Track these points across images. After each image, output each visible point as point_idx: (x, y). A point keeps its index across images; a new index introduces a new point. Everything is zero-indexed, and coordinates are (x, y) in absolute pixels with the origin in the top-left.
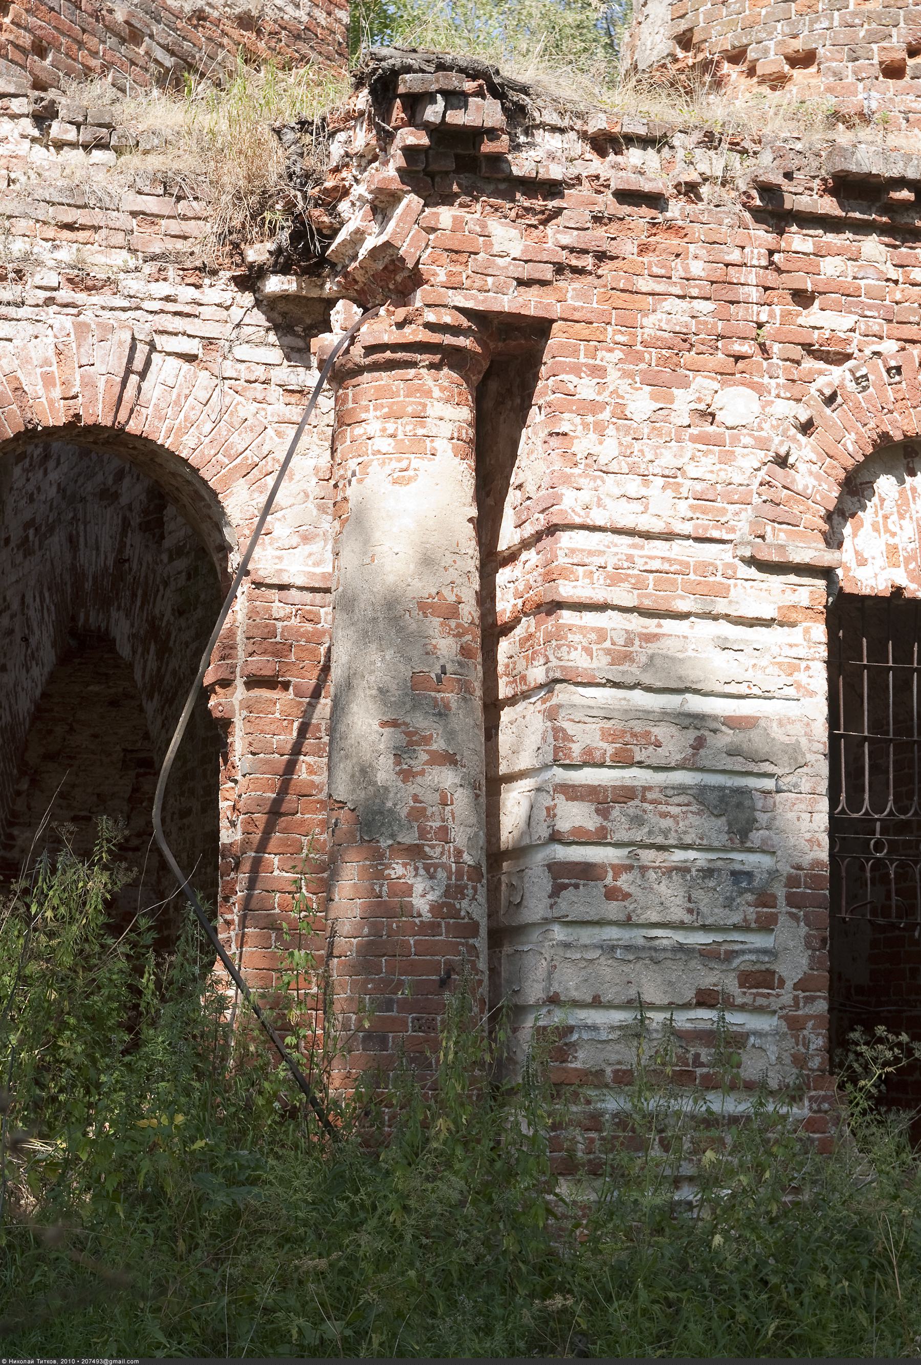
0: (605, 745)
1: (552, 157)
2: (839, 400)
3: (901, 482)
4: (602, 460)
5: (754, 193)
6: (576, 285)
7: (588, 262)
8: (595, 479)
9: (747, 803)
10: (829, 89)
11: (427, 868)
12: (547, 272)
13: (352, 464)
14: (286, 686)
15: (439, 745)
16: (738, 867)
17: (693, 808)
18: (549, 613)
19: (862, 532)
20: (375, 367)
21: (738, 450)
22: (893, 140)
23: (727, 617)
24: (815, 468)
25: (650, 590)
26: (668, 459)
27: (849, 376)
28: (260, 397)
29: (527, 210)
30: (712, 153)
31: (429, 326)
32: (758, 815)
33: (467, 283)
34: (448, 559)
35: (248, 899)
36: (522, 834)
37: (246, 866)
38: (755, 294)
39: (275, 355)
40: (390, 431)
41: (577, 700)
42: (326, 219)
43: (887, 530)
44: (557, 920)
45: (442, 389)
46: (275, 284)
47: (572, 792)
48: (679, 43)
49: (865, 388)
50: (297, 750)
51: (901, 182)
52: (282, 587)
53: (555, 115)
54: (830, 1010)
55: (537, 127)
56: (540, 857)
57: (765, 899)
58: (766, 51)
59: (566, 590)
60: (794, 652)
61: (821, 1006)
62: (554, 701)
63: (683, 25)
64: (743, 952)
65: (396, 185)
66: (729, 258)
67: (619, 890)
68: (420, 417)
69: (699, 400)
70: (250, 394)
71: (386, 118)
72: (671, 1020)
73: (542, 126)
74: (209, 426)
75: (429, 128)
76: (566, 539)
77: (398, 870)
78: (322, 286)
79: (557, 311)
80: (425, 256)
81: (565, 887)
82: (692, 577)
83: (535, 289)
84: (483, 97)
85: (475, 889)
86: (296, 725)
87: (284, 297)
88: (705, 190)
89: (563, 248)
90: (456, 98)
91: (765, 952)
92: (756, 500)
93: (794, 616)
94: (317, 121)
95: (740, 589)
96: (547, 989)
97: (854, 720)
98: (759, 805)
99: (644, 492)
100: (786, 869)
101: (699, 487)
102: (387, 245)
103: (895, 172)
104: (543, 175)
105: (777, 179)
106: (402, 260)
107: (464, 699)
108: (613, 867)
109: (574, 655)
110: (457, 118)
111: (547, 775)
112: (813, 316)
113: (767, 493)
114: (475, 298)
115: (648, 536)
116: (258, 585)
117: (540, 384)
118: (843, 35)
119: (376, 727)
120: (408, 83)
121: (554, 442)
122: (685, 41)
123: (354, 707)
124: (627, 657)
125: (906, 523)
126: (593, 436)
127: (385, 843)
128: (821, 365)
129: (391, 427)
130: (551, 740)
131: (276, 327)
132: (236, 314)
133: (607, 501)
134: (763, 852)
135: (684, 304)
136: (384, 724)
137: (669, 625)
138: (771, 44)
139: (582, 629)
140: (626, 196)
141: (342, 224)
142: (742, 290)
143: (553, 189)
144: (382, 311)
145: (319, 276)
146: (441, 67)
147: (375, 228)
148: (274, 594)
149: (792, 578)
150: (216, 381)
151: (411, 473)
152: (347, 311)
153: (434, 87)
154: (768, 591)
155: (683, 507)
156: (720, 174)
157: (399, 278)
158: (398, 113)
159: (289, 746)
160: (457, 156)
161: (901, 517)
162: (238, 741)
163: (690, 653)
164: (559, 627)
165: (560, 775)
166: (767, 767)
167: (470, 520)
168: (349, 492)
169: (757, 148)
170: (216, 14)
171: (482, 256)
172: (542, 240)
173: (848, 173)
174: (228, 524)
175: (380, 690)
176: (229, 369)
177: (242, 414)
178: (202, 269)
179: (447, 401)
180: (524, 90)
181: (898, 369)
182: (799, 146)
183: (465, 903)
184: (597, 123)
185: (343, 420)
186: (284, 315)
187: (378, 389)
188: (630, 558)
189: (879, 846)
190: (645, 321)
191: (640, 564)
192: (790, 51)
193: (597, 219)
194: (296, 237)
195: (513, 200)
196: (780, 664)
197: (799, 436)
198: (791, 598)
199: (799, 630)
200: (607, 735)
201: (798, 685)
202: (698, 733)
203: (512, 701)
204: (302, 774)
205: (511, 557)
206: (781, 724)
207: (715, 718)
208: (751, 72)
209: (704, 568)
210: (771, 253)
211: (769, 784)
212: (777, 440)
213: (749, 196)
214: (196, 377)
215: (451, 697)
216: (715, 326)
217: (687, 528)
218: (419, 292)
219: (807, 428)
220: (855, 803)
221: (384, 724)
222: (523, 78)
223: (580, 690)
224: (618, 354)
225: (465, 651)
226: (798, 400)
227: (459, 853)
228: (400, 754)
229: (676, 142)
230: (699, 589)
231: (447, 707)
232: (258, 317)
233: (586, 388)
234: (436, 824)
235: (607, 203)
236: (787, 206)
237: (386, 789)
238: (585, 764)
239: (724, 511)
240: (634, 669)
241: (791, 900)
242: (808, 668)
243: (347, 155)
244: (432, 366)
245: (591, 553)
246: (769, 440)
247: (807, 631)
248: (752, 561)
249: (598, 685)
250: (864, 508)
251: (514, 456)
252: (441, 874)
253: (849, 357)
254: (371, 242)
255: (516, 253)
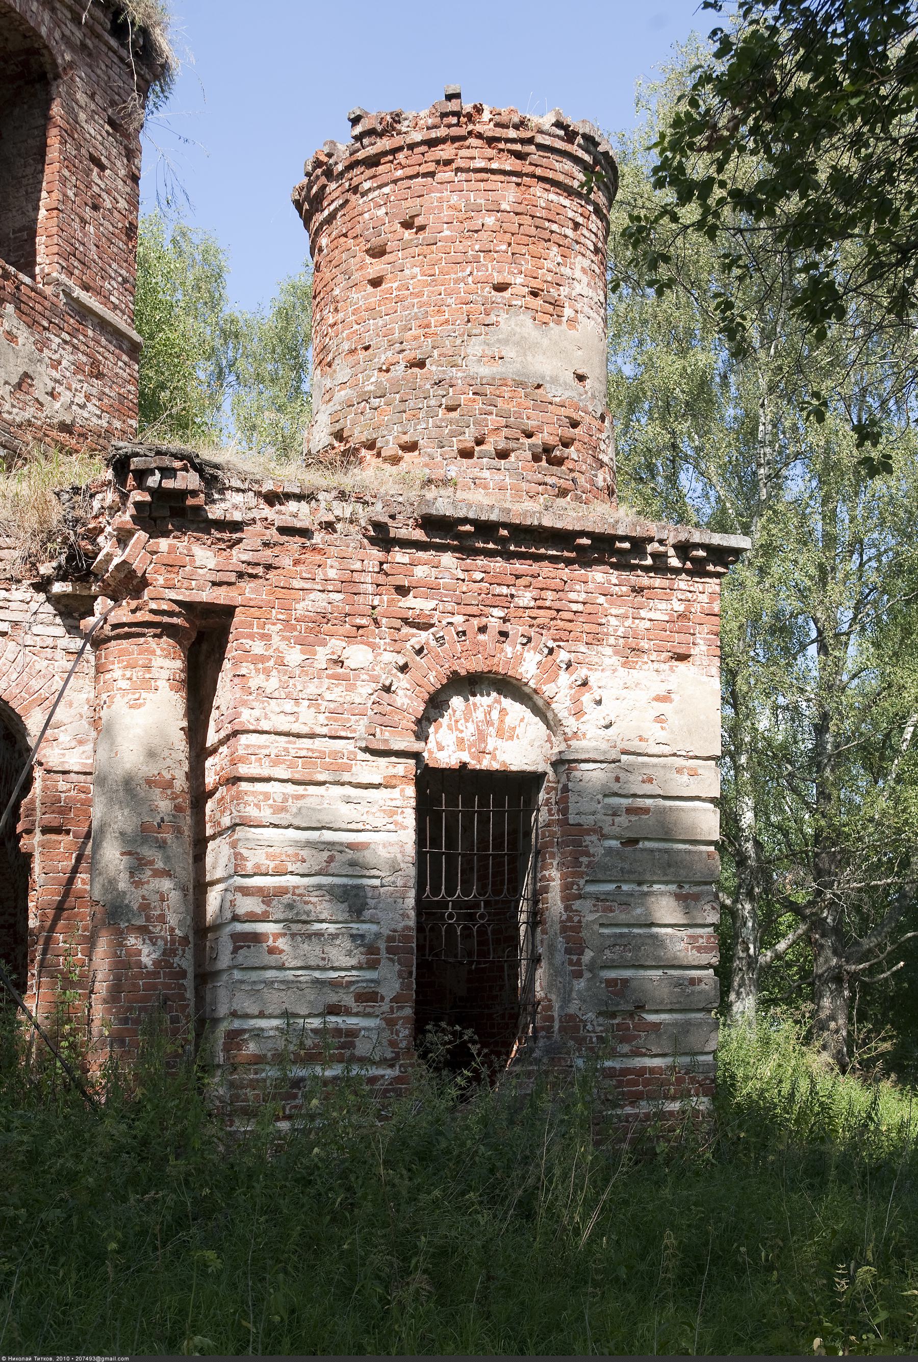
0: (268, 862)
1: (235, 507)
2: (425, 651)
3: (467, 700)
4: (268, 691)
5: (370, 528)
6: (252, 585)
7: (260, 570)
8: (263, 702)
9: (361, 894)
10: (426, 465)
11: (151, 939)
12: (232, 578)
13: (104, 696)
14: (68, 832)
15: (160, 865)
16: (355, 932)
17: (326, 898)
18: (233, 784)
19: (441, 731)
20: (118, 637)
21: (359, 683)
22: (460, 495)
23: (350, 783)
24: (409, 693)
25: (300, 768)
26: (312, 689)
27: (432, 637)
28: (50, 657)
29: (219, 539)
30: (344, 504)
31: (152, 611)
32: (369, 900)
33: (178, 584)
34: (166, 753)
35: (42, 961)
36: (217, 917)
37: (41, 941)
38: (370, 588)
39: (61, 631)
40: (128, 676)
41: (250, 835)
42: (90, 547)
43: (457, 729)
44: (235, 967)
45: (163, 650)
46: (58, 588)
47: (245, 891)
48: (336, 438)
49: (442, 645)
50: (75, 870)
51: (465, 521)
52: (64, 773)
53: (239, 482)
54: (415, 1013)
55: (227, 489)
56: (228, 930)
57: (371, 950)
58: (387, 442)
59: (243, 770)
60: (394, 803)
61: (408, 1011)
62: (235, 837)
63: (338, 427)
64: (358, 982)
65: (130, 525)
66: (353, 567)
67: (277, 948)
68: (148, 667)
69: (333, 653)
70: (43, 655)
71: (123, 484)
72: (325, 1022)
73: (230, 488)
74: (15, 676)
75: (150, 490)
76: (243, 739)
77: (132, 941)
78: (90, 589)
79: (239, 600)
80: (149, 569)
81: (242, 947)
82: (327, 760)
83: (224, 588)
84: (187, 471)
85: (184, 951)
86: (74, 855)
87: (64, 596)
88: (339, 526)
89: (243, 562)
90: (168, 472)
91: (372, 981)
92: (370, 713)
93: (394, 782)
94: (84, 487)
95: (359, 767)
96: (229, 1008)
97: (435, 843)
98: (370, 895)
99: (296, 709)
100: (386, 932)
101: (332, 705)
102: (124, 562)
103: (461, 514)
104: (229, 518)
105: (385, 519)
106: (135, 571)
107: (177, 837)
108: (273, 934)
109: (248, 809)
110: (168, 484)
111: (231, 881)
112: (410, 601)
113: (377, 708)
114: (183, 594)
115: (298, 736)
116: (49, 771)
117: (229, 645)
118: (434, 432)
119: (118, 855)
120: (135, 463)
121: (237, 680)
122: (339, 436)
123: (105, 844)
124: (284, 809)
125: (470, 725)
126: (262, 676)
127: (123, 925)
128: (414, 631)
129: (128, 674)
130: (233, 860)
131: (61, 614)
132: (34, 606)
133: (270, 715)
134: (372, 922)
135: (324, 595)
136: (123, 854)
137: (312, 789)
138: (391, 438)
139: (254, 793)
140: (284, 530)
141: (100, 550)
142: (362, 586)
143: (236, 526)
144: (124, 603)
145: (88, 582)
146: (159, 453)
147: (120, 552)
148: (60, 777)
149: (393, 759)
150: (20, 648)
151: (141, 701)
152: (103, 603)
153: (153, 465)
154: (377, 767)
155: (322, 718)
156: (348, 516)
157: (134, 583)
158: (131, 481)
159: (70, 868)
160: (171, 508)
161: (467, 721)
162: (37, 866)
163: (326, 806)
164: (239, 792)
165: (239, 881)
166: (375, 872)
167: (182, 729)
168: (102, 714)
169: (373, 500)
170: (39, 423)
171: (188, 568)
172: (229, 558)
173: (431, 515)
174: (29, 735)
175: (121, 833)
176: (29, 640)
177: (38, 667)
178: (10, 579)
179: (166, 657)
180: (217, 467)
181: (464, 633)
182: (400, 499)
183: (176, 959)
184: (267, 486)
185: (99, 670)
186: (66, 606)
187: (120, 650)
188: (286, 750)
189: (451, 916)
190: (297, 606)
191: (293, 753)
192: (402, 442)
193: (266, 545)
194: (70, 558)
195: (210, 534)
196: (384, 811)
197: (399, 674)
198: (392, 771)
199: (397, 790)
200: (269, 856)
201: (396, 823)
202: (330, 853)
203: (213, 837)
204: (78, 885)
205: (214, 751)
206: (384, 846)
207: (341, 844)
208: (379, 455)
209: (335, 754)
210: (381, 564)
211: (376, 882)
212: (384, 676)
213: (366, 530)
214: (6, 645)
215: (168, 836)
216: (344, 608)
217: (324, 730)
218: (146, 591)
219: (404, 668)
220: (436, 890)
221: (123, 854)
222: (217, 459)
223: (253, 830)
224: (279, 626)
225: (178, 808)
226: (399, 652)
227: (172, 930)
228: (132, 872)
229: (320, 497)
230: (331, 767)
231: (165, 842)
232: (49, 608)
233: (258, 648)
234: (157, 913)
235: (273, 534)
236: (392, 535)
237: (124, 892)
238: (255, 874)
239: (349, 720)
240: (288, 816)
241: (389, 950)
242: (403, 812)
243: (102, 507)
244: (155, 636)
245: (260, 747)
246: (379, 676)
247: (402, 791)
248: (366, 750)
249: (264, 826)
250: (442, 716)
251: (215, 690)
252: (160, 942)
253: (432, 625)
254: (116, 561)
255: (211, 565)
